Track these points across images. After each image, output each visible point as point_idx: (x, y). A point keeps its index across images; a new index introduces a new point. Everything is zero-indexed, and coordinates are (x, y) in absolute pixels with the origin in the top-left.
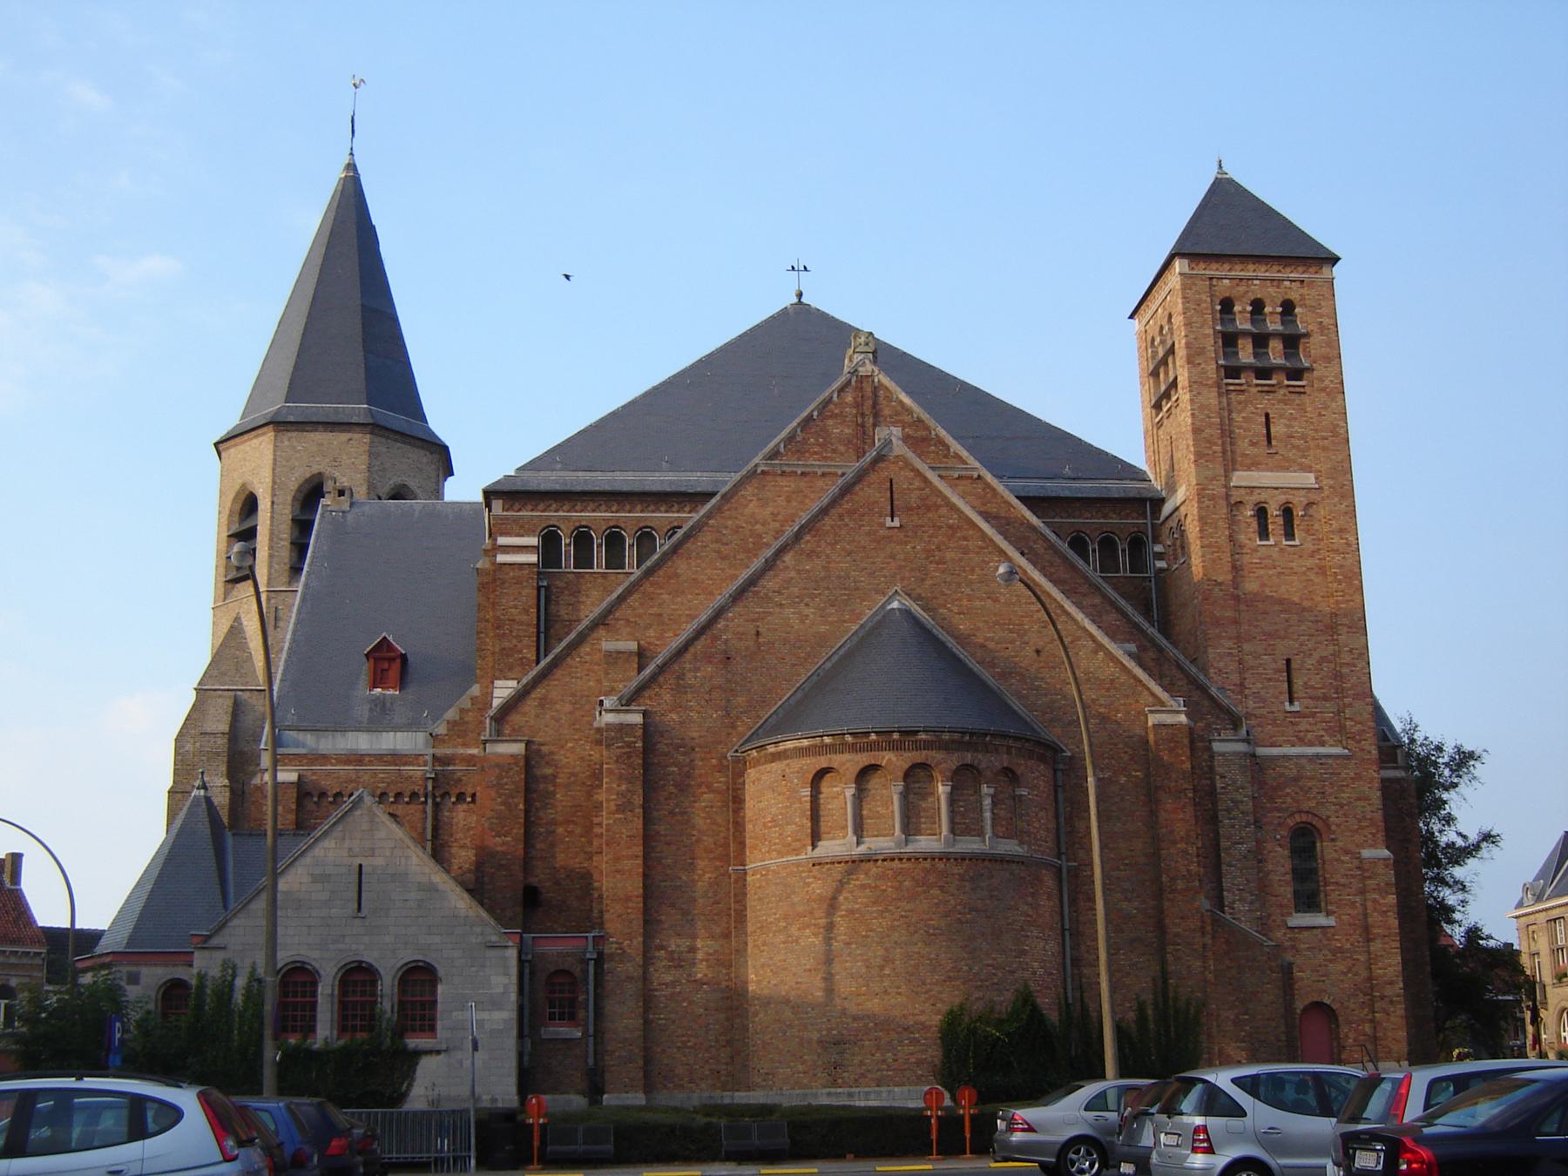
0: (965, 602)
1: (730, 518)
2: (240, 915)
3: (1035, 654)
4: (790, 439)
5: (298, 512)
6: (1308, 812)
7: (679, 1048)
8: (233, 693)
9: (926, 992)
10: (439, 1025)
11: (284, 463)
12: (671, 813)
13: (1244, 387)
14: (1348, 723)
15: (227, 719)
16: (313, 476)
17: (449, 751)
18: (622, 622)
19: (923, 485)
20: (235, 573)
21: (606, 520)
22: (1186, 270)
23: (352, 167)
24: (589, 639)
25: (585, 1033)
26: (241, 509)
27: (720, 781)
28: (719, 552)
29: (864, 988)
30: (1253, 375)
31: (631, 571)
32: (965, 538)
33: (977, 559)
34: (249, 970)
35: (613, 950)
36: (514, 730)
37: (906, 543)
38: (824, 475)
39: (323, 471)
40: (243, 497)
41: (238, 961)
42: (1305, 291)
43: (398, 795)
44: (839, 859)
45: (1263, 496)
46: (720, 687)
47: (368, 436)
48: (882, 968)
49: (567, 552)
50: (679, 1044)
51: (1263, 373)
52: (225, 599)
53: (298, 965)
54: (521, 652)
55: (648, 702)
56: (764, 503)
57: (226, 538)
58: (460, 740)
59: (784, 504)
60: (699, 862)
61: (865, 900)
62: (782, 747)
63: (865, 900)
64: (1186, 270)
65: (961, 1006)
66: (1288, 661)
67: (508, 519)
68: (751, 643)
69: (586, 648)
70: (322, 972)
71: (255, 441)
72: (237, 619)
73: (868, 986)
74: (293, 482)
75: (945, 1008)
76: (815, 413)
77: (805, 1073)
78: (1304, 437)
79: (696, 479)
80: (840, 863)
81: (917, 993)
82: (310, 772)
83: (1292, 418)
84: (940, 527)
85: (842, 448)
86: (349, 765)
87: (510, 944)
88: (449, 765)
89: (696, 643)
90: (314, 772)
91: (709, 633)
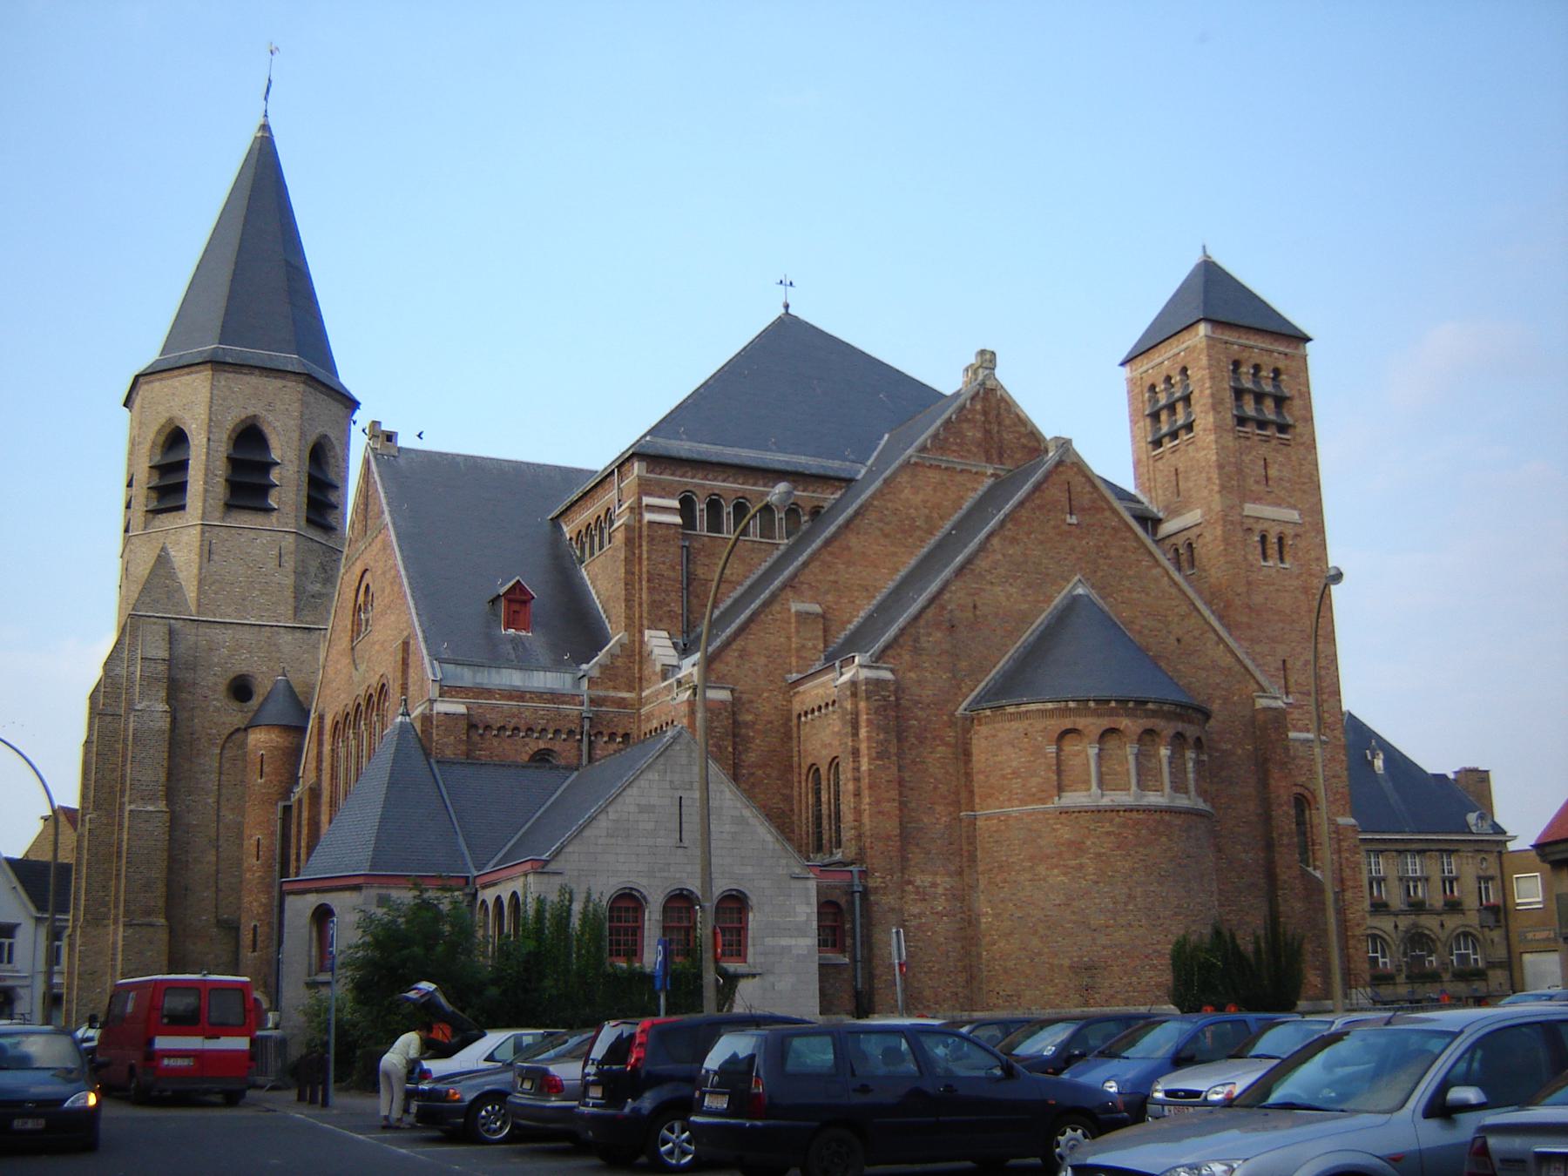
0: (1126, 594)
1: (891, 501)
2: (575, 842)
3: (1176, 643)
4: (935, 436)
5: (231, 451)
6: (1301, 786)
7: (925, 972)
8: (167, 621)
9: (1161, 925)
10: (750, 950)
11: (220, 402)
12: (914, 762)
13: (1249, 435)
14: (1326, 715)
15: (165, 645)
16: (247, 418)
17: (602, 693)
18: (806, 586)
19: (1091, 490)
20: (156, 503)
21: (735, 491)
22: (1210, 333)
23: (265, 127)
24: (779, 598)
25: (854, 959)
26: (164, 442)
27: (950, 735)
28: (881, 530)
29: (1112, 922)
30: (1255, 426)
31: (728, 536)
32: (1124, 539)
33: (1133, 557)
34: (584, 895)
35: (877, 884)
36: (718, 678)
37: (1083, 538)
38: (962, 471)
39: (257, 413)
40: (168, 430)
41: (574, 886)
42: (1288, 362)
43: (557, 732)
44: (1086, 808)
45: (1266, 525)
46: (947, 652)
47: (301, 385)
48: (1126, 904)
49: (701, 516)
50: (926, 970)
51: (1262, 424)
52: (145, 528)
53: (627, 891)
54: (669, 605)
55: (892, 660)
56: (916, 490)
57: (147, 469)
58: (610, 683)
59: (931, 492)
60: (936, 807)
61: (1110, 845)
62: (1023, 708)
63: (1110, 845)
64: (1210, 333)
65: (1184, 936)
66: (1284, 661)
67: (650, 481)
68: (970, 615)
69: (776, 607)
70: (650, 898)
71: (187, 377)
72: (163, 549)
73: (1115, 919)
74: (232, 419)
75: (1174, 939)
76: (954, 417)
77: (1057, 994)
78: (1289, 480)
79: (833, 466)
80: (1086, 812)
81: (1154, 926)
82: (476, 705)
83: (1282, 465)
84: (1106, 528)
85: (974, 449)
86: (511, 700)
87: (811, 875)
88: (601, 706)
89: (928, 610)
90: (480, 706)
91: (937, 602)
